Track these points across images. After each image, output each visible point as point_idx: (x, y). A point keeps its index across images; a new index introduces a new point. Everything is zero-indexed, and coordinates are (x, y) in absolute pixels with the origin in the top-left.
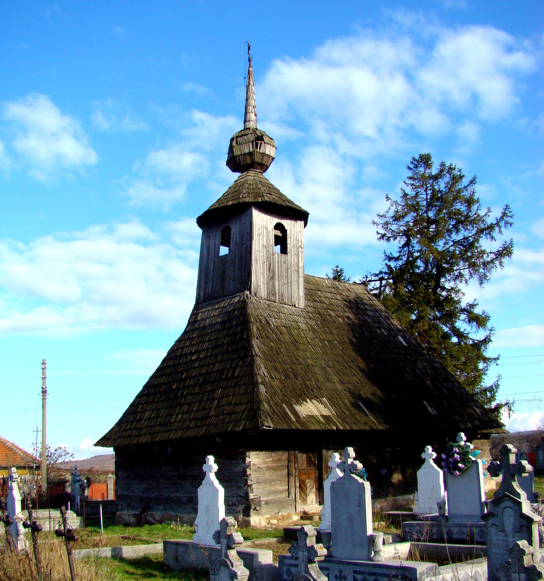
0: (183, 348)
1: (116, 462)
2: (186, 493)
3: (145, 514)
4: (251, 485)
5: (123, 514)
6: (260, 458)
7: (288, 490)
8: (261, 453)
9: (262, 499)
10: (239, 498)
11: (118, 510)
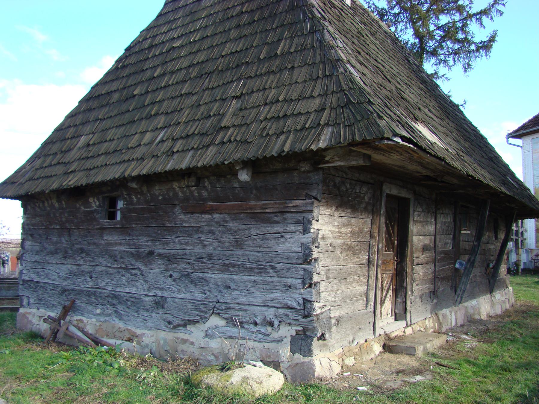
0: (154, 37)
1: (23, 225)
2: (150, 289)
3: (68, 318)
4: (316, 284)
5: (30, 313)
6: (332, 224)
7: (367, 295)
8: (336, 213)
9: (333, 314)
10: (282, 311)
11: (22, 306)
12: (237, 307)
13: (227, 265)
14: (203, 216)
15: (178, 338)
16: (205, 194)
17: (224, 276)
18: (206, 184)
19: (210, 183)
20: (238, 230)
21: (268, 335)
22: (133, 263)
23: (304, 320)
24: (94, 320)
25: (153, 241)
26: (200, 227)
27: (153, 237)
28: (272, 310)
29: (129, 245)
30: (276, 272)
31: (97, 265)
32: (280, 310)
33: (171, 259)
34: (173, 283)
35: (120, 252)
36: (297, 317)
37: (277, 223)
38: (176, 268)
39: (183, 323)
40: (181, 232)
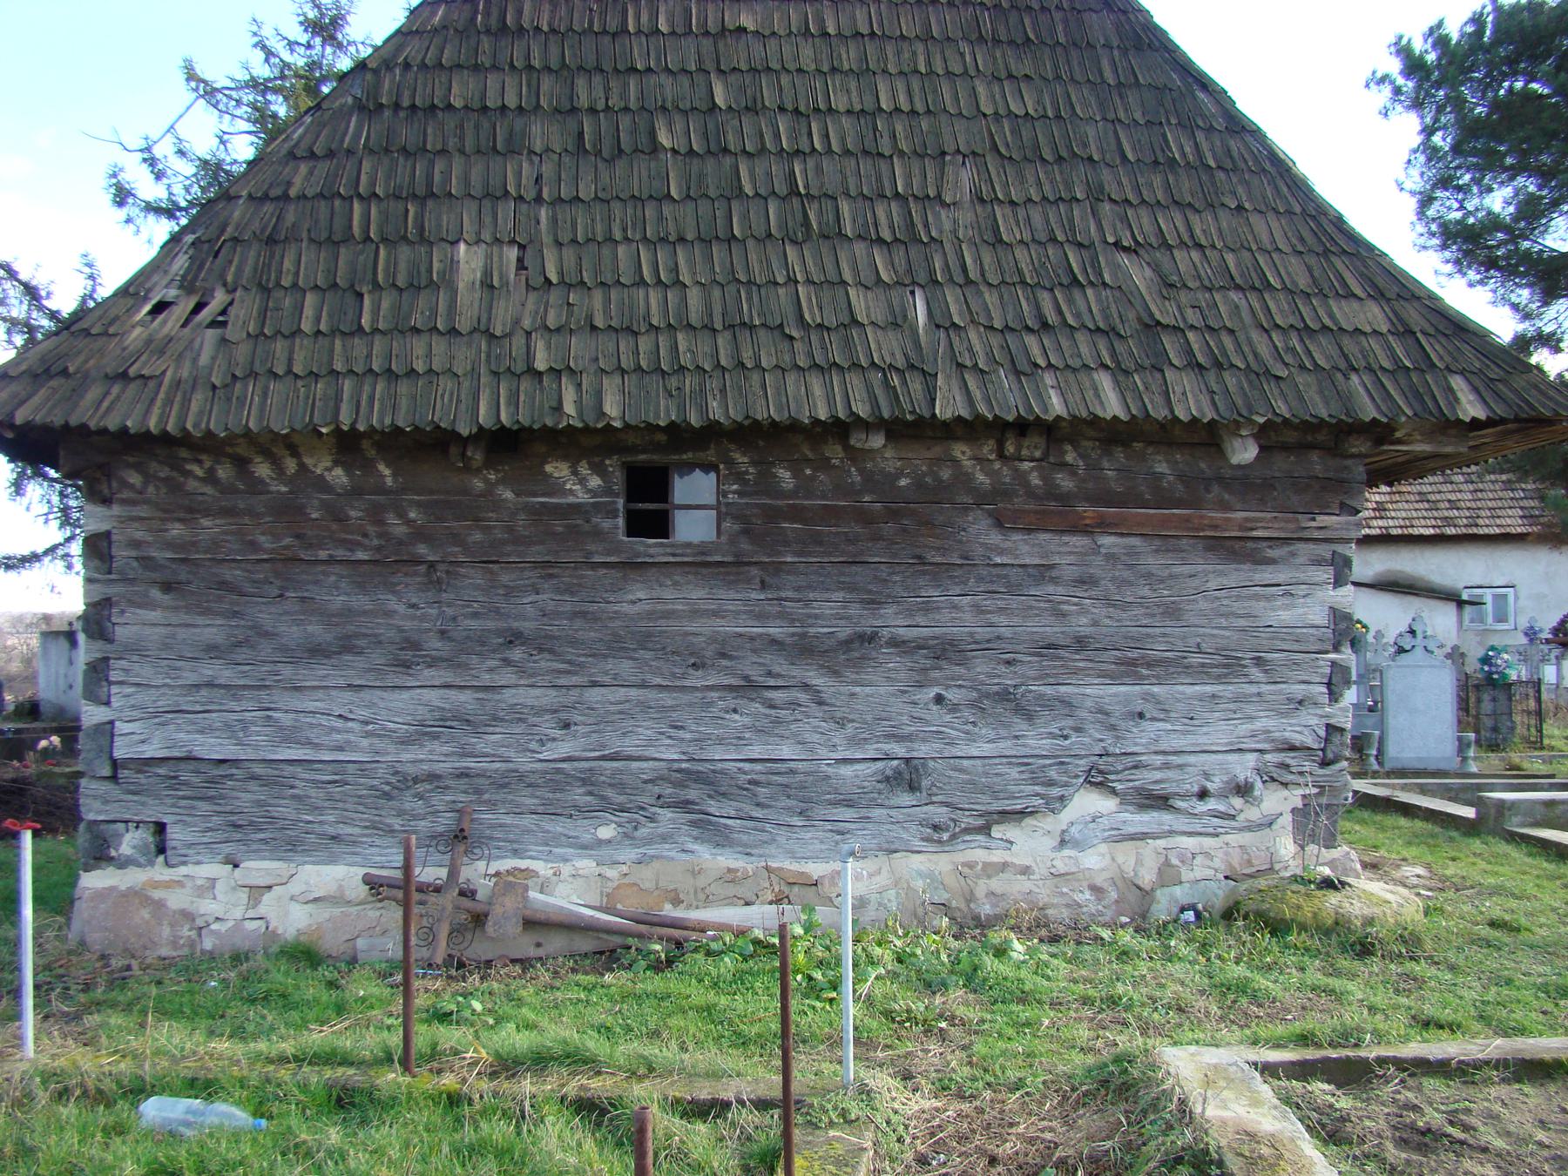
12: (1158, 760)
13: (1132, 663)
14: (1066, 539)
15: (970, 865)
16: (1065, 482)
17: (1122, 689)
18: (1070, 457)
19: (1081, 456)
20: (1171, 576)
21: (1233, 817)
22: (776, 669)
23: (1321, 772)
24: (586, 865)
25: (873, 603)
26: (1052, 567)
27: (870, 592)
28: (1251, 757)
29: (761, 617)
30: (1266, 672)
31: (594, 684)
32: (1268, 757)
33: (945, 651)
34: (948, 718)
35: (713, 639)
36: (1308, 766)
37: (1272, 561)
38: (960, 678)
39: (980, 822)
40: (980, 579)
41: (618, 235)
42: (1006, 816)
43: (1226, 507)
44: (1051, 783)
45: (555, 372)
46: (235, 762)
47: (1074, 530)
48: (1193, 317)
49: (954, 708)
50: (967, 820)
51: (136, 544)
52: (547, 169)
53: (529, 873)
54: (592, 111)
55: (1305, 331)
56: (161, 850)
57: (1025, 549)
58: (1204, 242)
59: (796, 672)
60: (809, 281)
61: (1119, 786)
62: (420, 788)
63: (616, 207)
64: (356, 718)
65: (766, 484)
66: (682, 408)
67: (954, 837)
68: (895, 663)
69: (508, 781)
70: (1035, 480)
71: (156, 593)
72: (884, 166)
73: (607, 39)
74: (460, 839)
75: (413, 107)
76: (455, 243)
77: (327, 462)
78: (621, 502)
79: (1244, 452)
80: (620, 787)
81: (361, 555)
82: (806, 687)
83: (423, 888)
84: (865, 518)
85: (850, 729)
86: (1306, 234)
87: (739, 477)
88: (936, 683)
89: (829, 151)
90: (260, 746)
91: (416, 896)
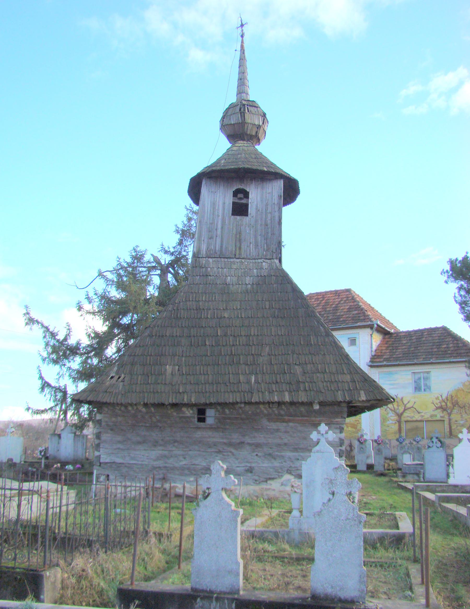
15: (263, 488)
16: (282, 412)
25: (244, 436)
31: (190, 450)
33: (258, 446)
41: (197, 364)
42: (270, 479)
43: (316, 417)
44: (279, 472)
45: (184, 393)
46: (123, 463)
47: (283, 422)
48: (308, 380)
49: (260, 457)
50: (262, 479)
51: (106, 422)
52: (185, 349)
53: (177, 487)
54: (194, 336)
55: (331, 382)
56: (108, 480)
57: (274, 426)
58: (314, 362)
59: (229, 449)
60: (232, 373)
61: (294, 474)
62: (157, 469)
63: (197, 357)
64: (146, 456)
65: (224, 413)
66: (206, 399)
67: (259, 483)
68: (248, 447)
69: (173, 469)
70: (276, 412)
71: (109, 431)
72: (250, 347)
73: (197, 320)
74: (164, 479)
75: (159, 336)
76: (166, 365)
77: (142, 407)
78: (196, 416)
79: (316, 407)
80: (195, 470)
81: (147, 425)
82: (231, 452)
83: (156, 488)
84: (242, 419)
85: (239, 460)
86: (338, 359)
87: (219, 411)
88: (256, 451)
89: (240, 345)
90: (127, 460)
91: (155, 489)
